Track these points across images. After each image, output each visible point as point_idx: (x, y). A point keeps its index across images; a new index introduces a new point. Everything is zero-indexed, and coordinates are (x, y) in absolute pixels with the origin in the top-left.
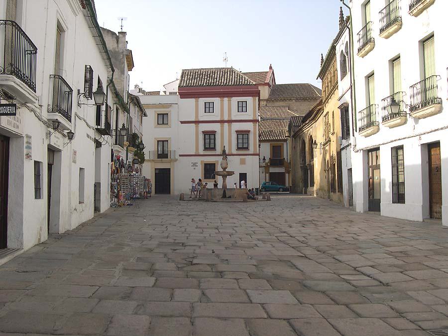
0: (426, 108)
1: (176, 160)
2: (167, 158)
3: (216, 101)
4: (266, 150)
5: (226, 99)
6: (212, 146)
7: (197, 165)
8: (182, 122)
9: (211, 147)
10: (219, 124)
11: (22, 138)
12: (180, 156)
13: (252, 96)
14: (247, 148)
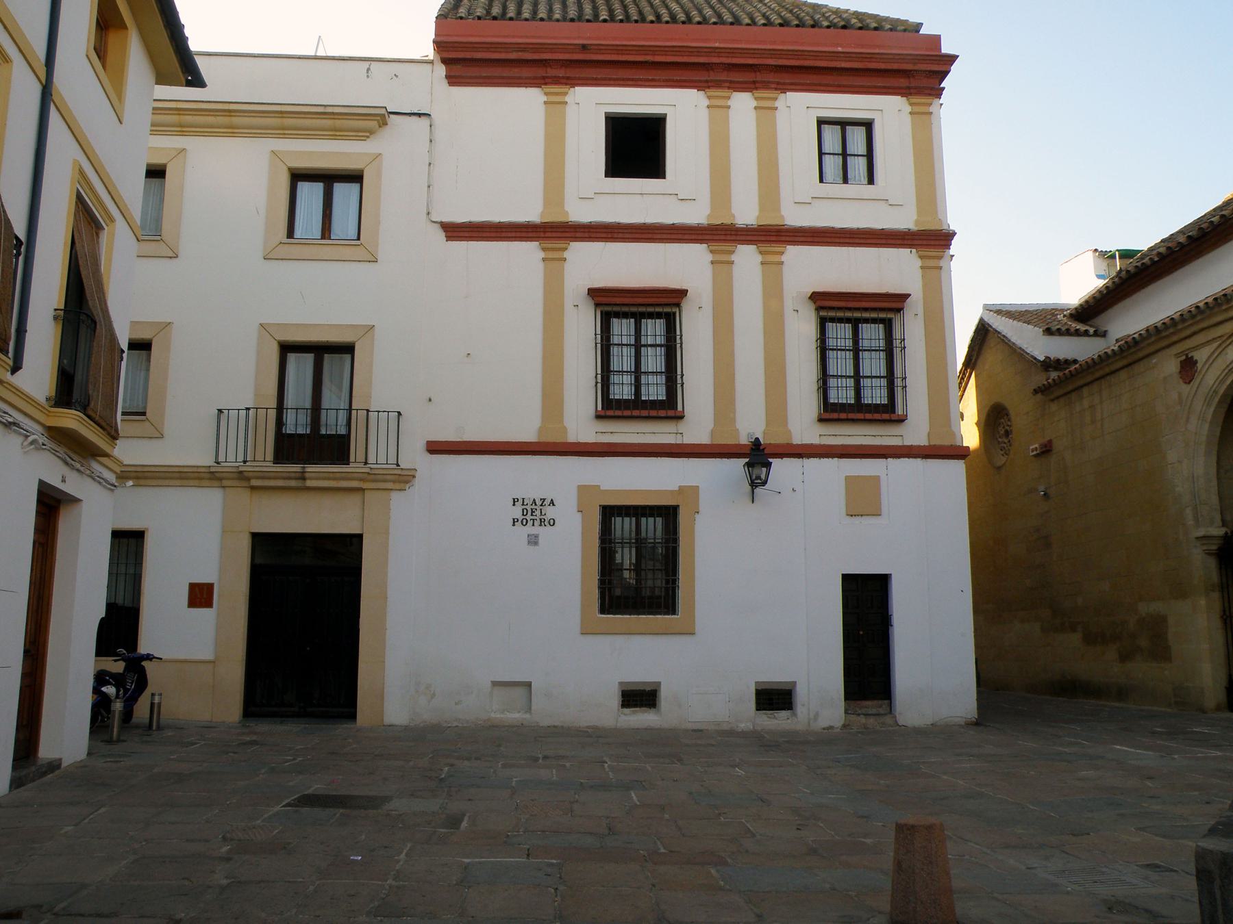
1: (404, 479)
5: (742, 104)
6: (654, 390)
7: (550, 512)
8: (455, 231)
12: (435, 448)
14: (888, 413)
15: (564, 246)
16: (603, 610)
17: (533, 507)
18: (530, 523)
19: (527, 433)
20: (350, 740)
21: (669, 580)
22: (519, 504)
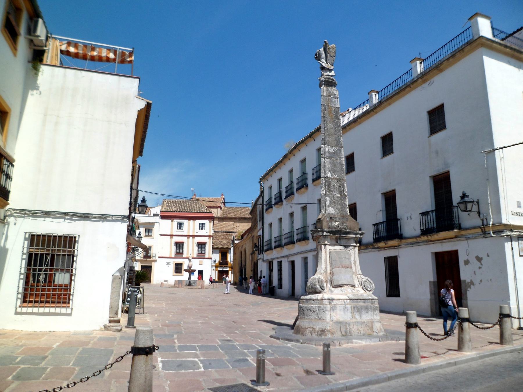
3: (185, 222)
4: (217, 257)
5: (192, 221)
7: (170, 264)
8: (161, 235)
9: (202, 252)
11: (517, 239)
12: (159, 257)
13: (188, 220)
16: (175, 273)
19: (168, 256)
20: (342, 194)
21: (52, 297)
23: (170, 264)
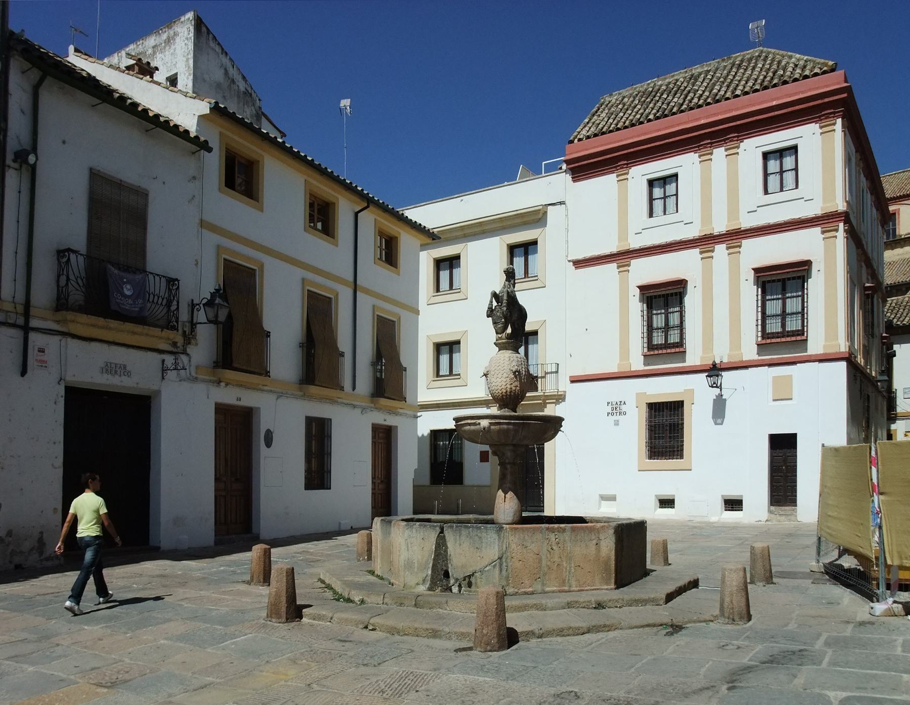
0: (870, 235)
2: (791, 376)
5: (719, 153)
7: (624, 408)
8: (579, 264)
10: (694, 254)
12: (574, 380)
15: (739, 244)
17: (616, 406)
18: (615, 414)
19: (613, 369)
22: (610, 405)
23: (624, 408)
